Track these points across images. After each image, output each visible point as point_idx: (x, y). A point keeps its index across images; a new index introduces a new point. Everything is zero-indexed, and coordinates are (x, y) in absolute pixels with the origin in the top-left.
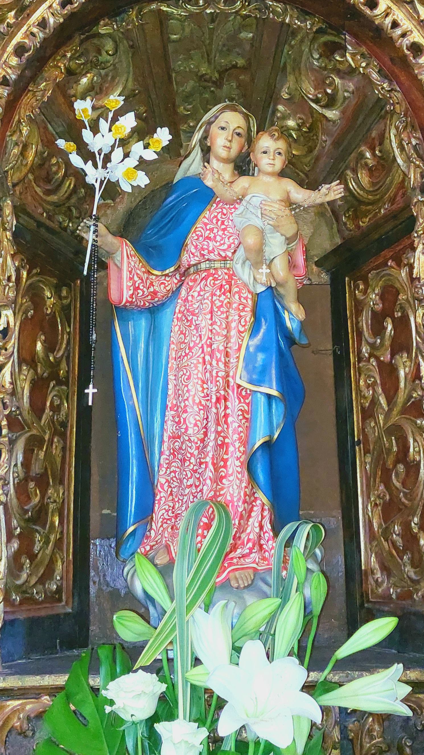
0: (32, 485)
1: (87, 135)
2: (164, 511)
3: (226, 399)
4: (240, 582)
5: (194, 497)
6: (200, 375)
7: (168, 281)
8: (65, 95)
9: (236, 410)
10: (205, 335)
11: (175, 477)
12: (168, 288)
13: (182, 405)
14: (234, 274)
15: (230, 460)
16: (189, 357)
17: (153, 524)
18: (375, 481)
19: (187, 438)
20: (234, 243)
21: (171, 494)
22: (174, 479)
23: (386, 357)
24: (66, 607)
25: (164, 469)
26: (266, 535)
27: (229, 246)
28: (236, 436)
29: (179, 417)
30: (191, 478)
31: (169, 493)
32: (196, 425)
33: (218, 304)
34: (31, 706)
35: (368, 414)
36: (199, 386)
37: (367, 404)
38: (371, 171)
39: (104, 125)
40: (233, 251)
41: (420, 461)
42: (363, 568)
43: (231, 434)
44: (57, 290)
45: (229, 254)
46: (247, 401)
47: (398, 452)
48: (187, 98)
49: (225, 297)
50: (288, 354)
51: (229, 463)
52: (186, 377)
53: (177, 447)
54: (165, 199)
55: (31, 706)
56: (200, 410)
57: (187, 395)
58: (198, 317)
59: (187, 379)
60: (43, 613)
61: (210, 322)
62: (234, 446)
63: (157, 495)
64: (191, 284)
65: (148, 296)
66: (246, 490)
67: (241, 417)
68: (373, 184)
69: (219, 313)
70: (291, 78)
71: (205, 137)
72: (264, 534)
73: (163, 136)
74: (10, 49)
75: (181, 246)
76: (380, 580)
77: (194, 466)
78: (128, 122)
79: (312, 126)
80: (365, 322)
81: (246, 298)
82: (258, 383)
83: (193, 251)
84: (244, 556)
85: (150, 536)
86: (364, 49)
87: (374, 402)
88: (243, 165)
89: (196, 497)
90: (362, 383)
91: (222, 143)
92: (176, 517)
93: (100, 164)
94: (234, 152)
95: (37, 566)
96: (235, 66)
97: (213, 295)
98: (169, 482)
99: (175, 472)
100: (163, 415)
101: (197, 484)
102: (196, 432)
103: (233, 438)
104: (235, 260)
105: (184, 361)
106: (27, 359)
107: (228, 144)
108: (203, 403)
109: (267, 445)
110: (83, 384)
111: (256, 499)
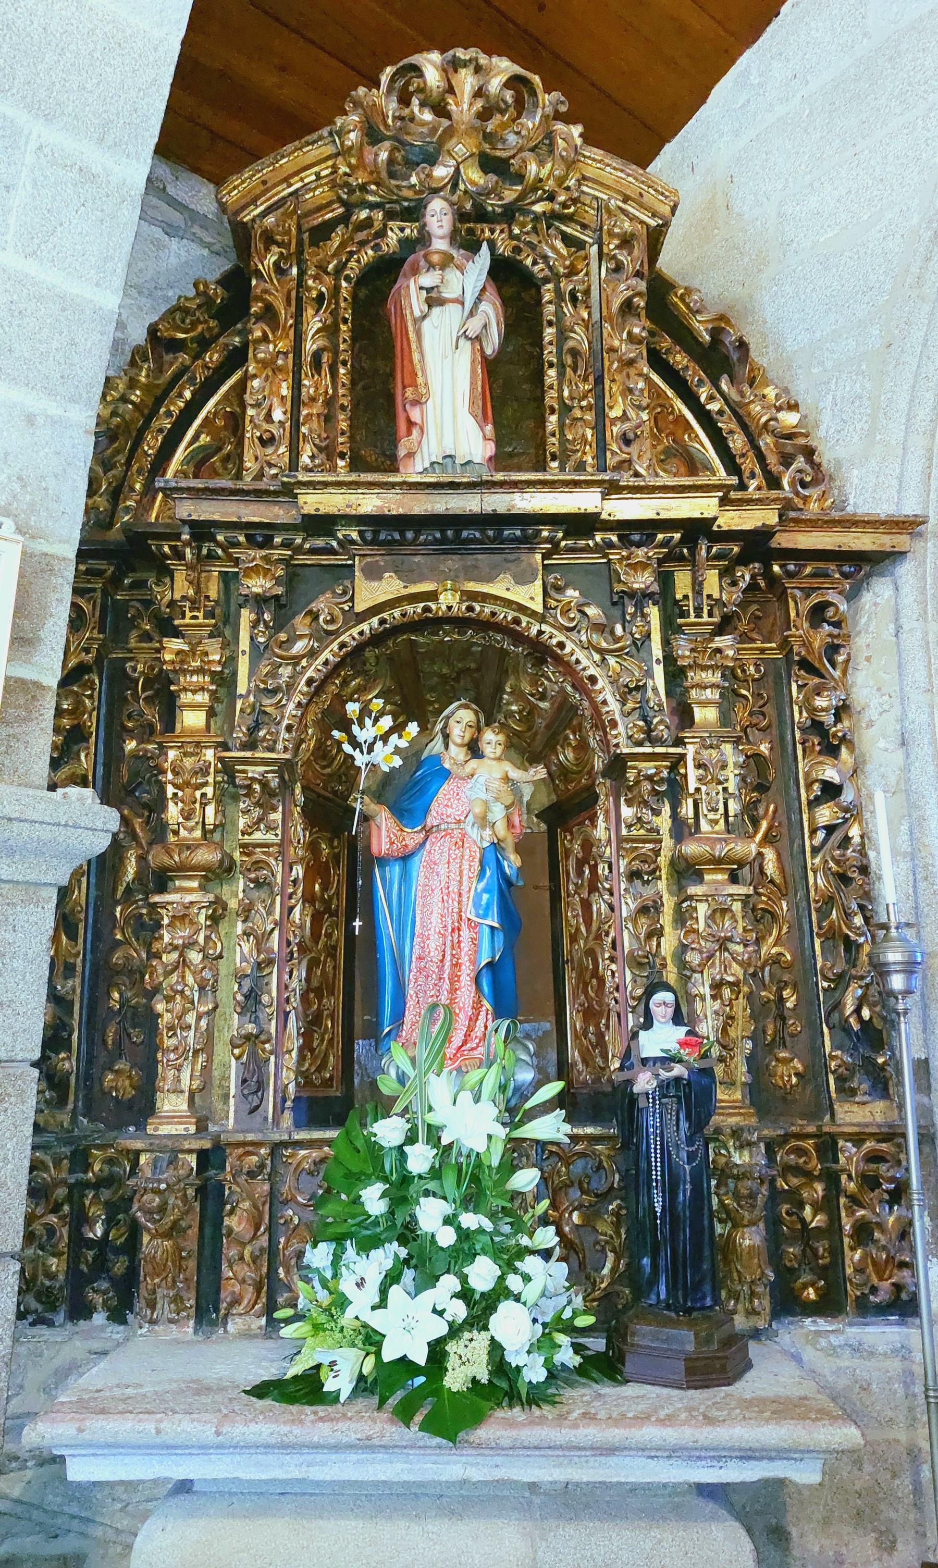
0: (312, 995)
1: (355, 729)
3: (459, 930)
8: (341, 700)
23: (585, 895)
24: (336, 1092)
28: (467, 958)
34: (315, 1154)
35: (574, 939)
38: (575, 749)
39: (368, 722)
44: (331, 841)
48: (432, 689)
50: (507, 894)
54: (415, 772)
55: (315, 1154)
60: (320, 1095)
68: (577, 759)
70: (512, 677)
71: (445, 727)
73: (413, 728)
74: (303, 682)
75: (427, 811)
78: (387, 722)
79: (530, 713)
80: (572, 864)
82: (485, 916)
84: (473, 1049)
86: (561, 669)
87: (578, 929)
88: (474, 749)
91: (458, 732)
93: (365, 751)
94: (467, 739)
95: (317, 1057)
96: (469, 669)
97: (450, 849)
100: (412, 942)
103: (464, 959)
106: (309, 898)
109: (489, 965)
110: (350, 919)
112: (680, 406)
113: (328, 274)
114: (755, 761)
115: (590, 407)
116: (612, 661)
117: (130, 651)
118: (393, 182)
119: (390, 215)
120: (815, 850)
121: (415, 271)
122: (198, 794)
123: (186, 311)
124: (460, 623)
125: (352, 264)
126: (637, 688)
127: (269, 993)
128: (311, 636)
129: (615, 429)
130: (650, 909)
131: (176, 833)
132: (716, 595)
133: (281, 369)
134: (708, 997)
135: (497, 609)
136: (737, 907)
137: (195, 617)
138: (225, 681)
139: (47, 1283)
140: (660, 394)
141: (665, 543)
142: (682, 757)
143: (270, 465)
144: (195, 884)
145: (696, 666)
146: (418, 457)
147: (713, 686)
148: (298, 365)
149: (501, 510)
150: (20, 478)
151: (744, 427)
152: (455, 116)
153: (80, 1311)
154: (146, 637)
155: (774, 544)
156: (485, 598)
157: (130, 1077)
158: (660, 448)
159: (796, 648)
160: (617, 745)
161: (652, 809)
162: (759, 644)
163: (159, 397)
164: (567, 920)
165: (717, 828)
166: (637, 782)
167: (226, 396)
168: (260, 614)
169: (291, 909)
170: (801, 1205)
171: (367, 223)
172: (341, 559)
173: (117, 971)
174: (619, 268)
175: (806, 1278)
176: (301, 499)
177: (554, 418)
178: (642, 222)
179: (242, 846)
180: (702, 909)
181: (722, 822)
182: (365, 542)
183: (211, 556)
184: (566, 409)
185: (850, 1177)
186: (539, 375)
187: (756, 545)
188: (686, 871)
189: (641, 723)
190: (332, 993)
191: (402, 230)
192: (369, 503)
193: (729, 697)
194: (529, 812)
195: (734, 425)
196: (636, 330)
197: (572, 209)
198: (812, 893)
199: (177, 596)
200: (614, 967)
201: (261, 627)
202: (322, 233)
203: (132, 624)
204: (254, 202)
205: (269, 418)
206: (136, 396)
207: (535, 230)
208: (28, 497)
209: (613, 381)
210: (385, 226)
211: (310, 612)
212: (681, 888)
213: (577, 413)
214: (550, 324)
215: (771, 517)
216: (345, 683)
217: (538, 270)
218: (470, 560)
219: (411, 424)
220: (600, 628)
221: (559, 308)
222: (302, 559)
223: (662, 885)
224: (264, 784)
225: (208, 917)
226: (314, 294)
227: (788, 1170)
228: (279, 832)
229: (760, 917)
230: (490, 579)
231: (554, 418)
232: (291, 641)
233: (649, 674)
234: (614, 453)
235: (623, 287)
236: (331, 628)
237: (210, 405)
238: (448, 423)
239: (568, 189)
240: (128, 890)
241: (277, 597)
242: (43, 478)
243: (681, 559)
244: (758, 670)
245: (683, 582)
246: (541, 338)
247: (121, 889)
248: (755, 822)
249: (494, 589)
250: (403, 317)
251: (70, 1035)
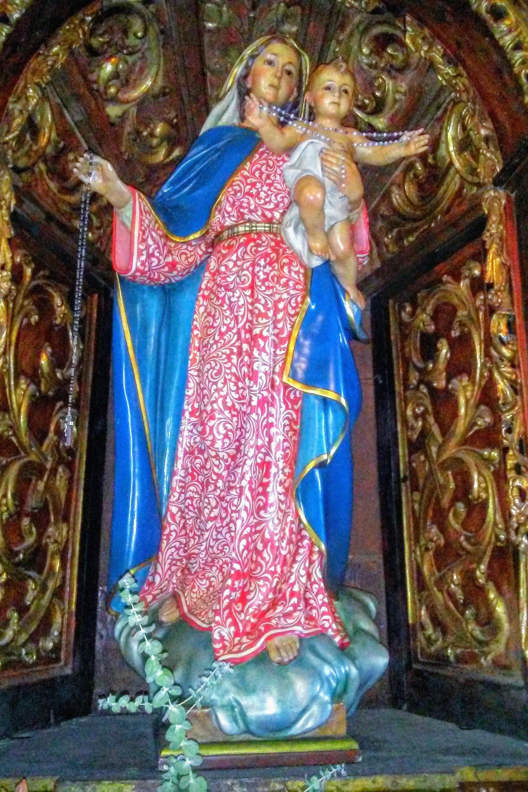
0: (26, 521)
2: (173, 550)
4: (284, 654)
5: (219, 533)
6: (234, 370)
7: (191, 252)
9: (281, 420)
10: (243, 316)
11: (192, 505)
12: (191, 260)
13: (209, 408)
14: (282, 241)
15: (271, 485)
16: (219, 345)
17: (159, 566)
18: (425, 522)
19: (213, 454)
20: (282, 202)
21: (184, 527)
22: (191, 508)
25: (176, 494)
26: (315, 586)
27: (277, 205)
28: (280, 454)
29: (203, 424)
30: (216, 507)
31: (181, 525)
32: (226, 436)
33: (262, 276)
35: (418, 446)
36: (232, 384)
37: (415, 437)
40: (281, 211)
41: (487, 500)
42: (410, 621)
43: (274, 451)
45: (277, 215)
46: (296, 407)
47: (455, 491)
49: (270, 268)
51: (269, 489)
52: (215, 371)
53: (198, 466)
56: (233, 416)
57: (216, 395)
58: (234, 292)
59: (216, 375)
61: (250, 300)
62: (277, 466)
63: (166, 528)
64: (224, 252)
65: (164, 267)
66: (293, 526)
67: (287, 428)
68: (422, 198)
69: (263, 288)
72: (311, 585)
76: (433, 637)
77: (222, 491)
81: (297, 273)
83: (229, 209)
84: (288, 615)
85: (153, 583)
86: (427, 32)
87: (424, 434)
89: (220, 533)
90: (409, 412)
91: (266, 83)
92: (189, 557)
94: (283, 93)
97: (253, 265)
98: (183, 512)
99: (192, 498)
101: (224, 515)
102: (226, 445)
104: (285, 222)
105: (212, 350)
107: (275, 82)
108: (237, 406)
111: (303, 538)
164: (405, 421)
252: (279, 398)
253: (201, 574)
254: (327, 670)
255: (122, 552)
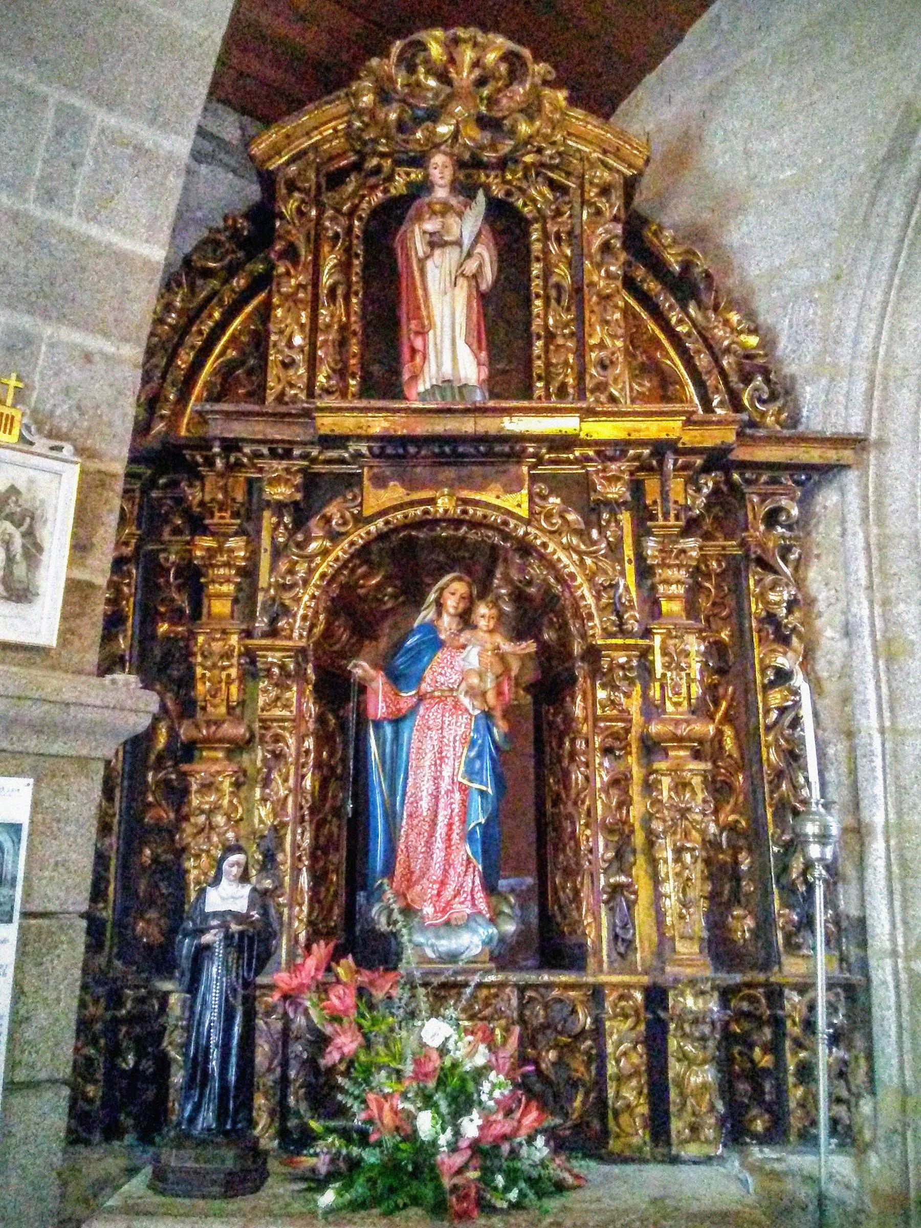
75: (420, 679)
88: (466, 619)
91: (451, 603)
112: (652, 326)
113: (343, 214)
114: (717, 649)
115: (573, 334)
116: (589, 561)
117: (162, 543)
118: (401, 136)
119: (398, 163)
120: (768, 729)
121: (419, 218)
122: (224, 675)
123: (217, 244)
124: (457, 523)
125: (364, 205)
126: (611, 586)
127: (284, 851)
128: (323, 538)
129: (593, 355)
130: (620, 782)
131: (204, 708)
132: (681, 501)
133: (301, 301)
134: (670, 860)
135: (489, 512)
136: (697, 781)
137: (222, 518)
138: (249, 573)
139: (87, 1108)
140: (636, 316)
141: (638, 457)
142: (649, 649)
143: (292, 386)
144: (220, 755)
145: (664, 565)
146: (420, 382)
147: (678, 582)
148: (316, 297)
149: (493, 431)
150: (79, 408)
151: (710, 348)
152: (456, 84)
153: (112, 1132)
154: (177, 531)
155: (732, 457)
156: (476, 503)
157: (158, 925)
158: (635, 363)
159: (753, 549)
160: (593, 636)
161: (625, 693)
162: (722, 542)
163: (192, 317)
165: (680, 709)
166: (611, 669)
167: (249, 316)
168: (281, 516)
169: (303, 777)
170: (751, 1047)
171: (378, 170)
172: (353, 468)
173: (148, 830)
174: (599, 212)
175: (755, 1111)
176: (319, 421)
177: (539, 343)
178: (618, 171)
179: (262, 720)
180: (666, 782)
181: (685, 703)
182: (374, 456)
183: (239, 465)
184: (550, 337)
185: (794, 1023)
186: (528, 303)
187: (717, 460)
188: (651, 748)
189: (613, 618)
190: (337, 849)
191: (408, 174)
192: (378, 425)
193: (694, 590)
194: (517, 685)
195: (700, 345)
196: (613, 268)
197: (557, 161)
198: (765, 767)
199: (207, 498)
200: (588, 832)
201: (281, 529)
202: (336, 179)
203: (166, 520)
204: (279, 153)
205: (290, 345)
206: (172, 318)
207: (526, 177)
208: (86, 424)
209: (592, 312)
210: (393, 171)
211: (324, 516)
212: (649, 763)
213: (560, 341)
214: (538, 259)
215: (730, 437)
216: (353, 571)
217: (528, 211)
218: (465, 471)
219: (413, 351)
220: (579, 533)
221: (546, 246)
222: (319, 468)
223: (632, 760)
224: (282, 667)
225: (232, 784)
226: (330, 233)
227: (741, 1015)
228: (294, 708)
229: (719, 789)
230: (481, 488)
231: (539, 343)
232: (308, 540)
233: (623, 573)
234: (592, 376)
235: (601, 230)
236: (343, 529)
237: (237, 323)
238: (448, 351)
239: (554, 143)
240: (160, 758)
241: (296, 503)
242: (98, 407)
243: (651, 469)
244: (719, 565)
245: (652, 485)
246: (529, 272)
247: (153, 757)
248: (717, 703)
249: (488, 497)
250: (408, 259)
251: (107, 888)
252: (456, 788)
253: (417, 882)
254: (481, 930)
255: (374, 871)
